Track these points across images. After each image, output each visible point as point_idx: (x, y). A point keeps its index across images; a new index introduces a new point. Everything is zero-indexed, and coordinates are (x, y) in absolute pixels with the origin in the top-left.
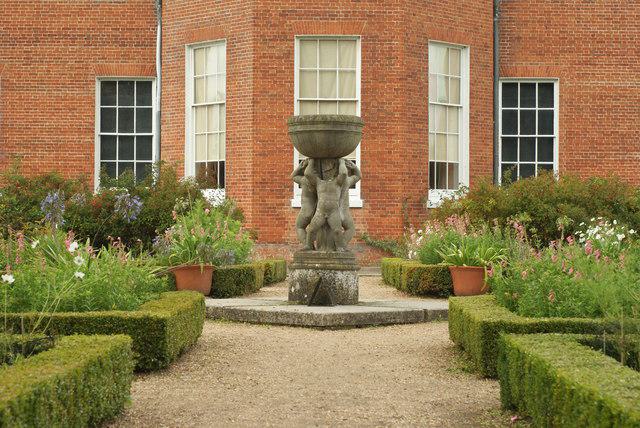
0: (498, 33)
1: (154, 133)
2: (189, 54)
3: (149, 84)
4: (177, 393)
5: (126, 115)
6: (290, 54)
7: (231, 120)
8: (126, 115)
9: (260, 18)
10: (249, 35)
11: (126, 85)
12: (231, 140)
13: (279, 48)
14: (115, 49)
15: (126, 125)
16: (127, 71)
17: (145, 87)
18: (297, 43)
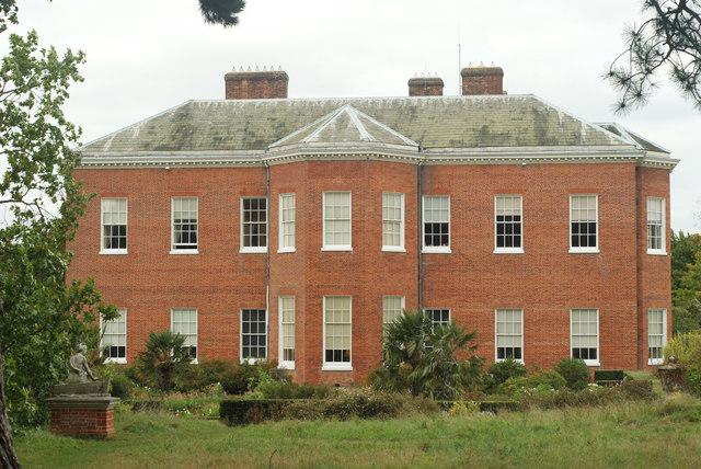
0: (421, 287)
1: (266, 346)
2: (280, 300)
3: (264, 311)
4: (624, 445)
5: (254, 325)
6: (321, 304)
7: (297, 332)
8: (254, 325)
9: (308, 288)
10: (304, 296)
11: (254, 312)
12: (297, 341)
13: (316, 301)
14: (249, 296)
15: (254, 331)
16: (254, 305)
17: (262, 313)
18: (324, 299)
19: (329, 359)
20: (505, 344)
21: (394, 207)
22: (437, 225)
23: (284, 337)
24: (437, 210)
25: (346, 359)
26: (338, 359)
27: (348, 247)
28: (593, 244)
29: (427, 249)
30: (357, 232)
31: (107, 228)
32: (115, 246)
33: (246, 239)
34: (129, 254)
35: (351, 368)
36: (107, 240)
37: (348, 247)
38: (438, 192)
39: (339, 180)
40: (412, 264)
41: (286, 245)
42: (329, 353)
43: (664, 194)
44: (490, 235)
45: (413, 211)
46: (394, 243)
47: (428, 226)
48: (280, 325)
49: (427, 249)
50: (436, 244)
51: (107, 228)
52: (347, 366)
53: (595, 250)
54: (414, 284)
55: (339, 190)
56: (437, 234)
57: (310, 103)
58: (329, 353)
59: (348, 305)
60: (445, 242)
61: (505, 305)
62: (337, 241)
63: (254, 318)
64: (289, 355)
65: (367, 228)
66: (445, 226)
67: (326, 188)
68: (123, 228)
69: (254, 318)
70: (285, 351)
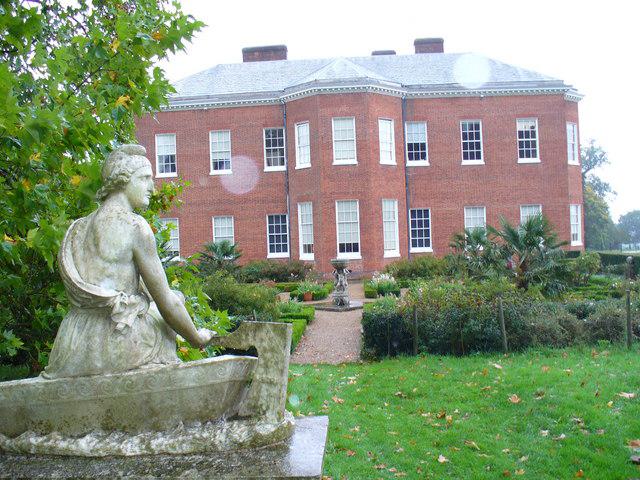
0: (408, 193)
2: (299, 207)
11: (277, 217)
17: (284, 217)
19: (342, 250)
20: (219, 157)
21: (386, 130)
22: (417, 145)
23: (305, 236)
24: (417, 133)
25: (356, 250)
26: (349, 250)
27: (355, 162)
28: (534, 156)
29: (410, 163)
30: (360, 148)
31: (160, 157)
32: (167, 171)
33: (272, 247)
34: (234, 172)
35: (360, 257)
36: (161, 167)
37: (355, 162)
38: (417, 119)
39: (344, 109)
40: (401, 174)
41: (303, 160)
42: (342, 246)
43: (575, 120)
44: (458, 151)
45: (400, 135)
46: (387, 156)
47: (410, 145)
48: (300, 227)
49: (410, 163)
50: (417, 158)
51: (160, 157)
52: (357, 255)
53: (481, 162)
54: (403, 190)
55: (346, 116)
56: (416, 151)
57: (310, 62)
58: (342, 246)
59: (355, 208)
60: (424, 157)
61: (471, 204)
62: (344, 155)
63: (277, 221)
64: (308, 249)
65: (367, 146)
66: (423, 145)
67: (334, 115)
68: (172, 157)
69: (277, 221)
70: (305, 246)
